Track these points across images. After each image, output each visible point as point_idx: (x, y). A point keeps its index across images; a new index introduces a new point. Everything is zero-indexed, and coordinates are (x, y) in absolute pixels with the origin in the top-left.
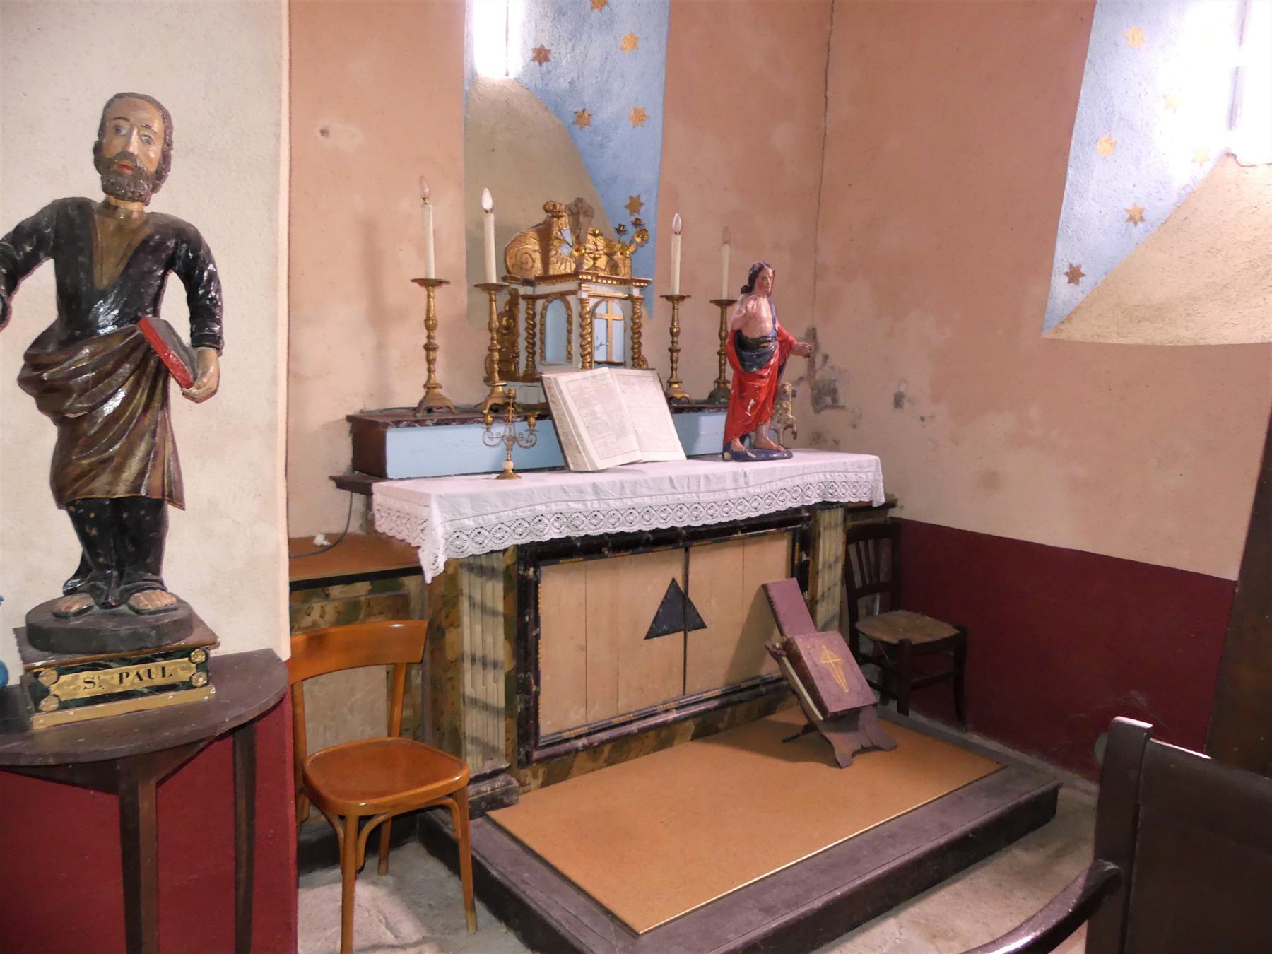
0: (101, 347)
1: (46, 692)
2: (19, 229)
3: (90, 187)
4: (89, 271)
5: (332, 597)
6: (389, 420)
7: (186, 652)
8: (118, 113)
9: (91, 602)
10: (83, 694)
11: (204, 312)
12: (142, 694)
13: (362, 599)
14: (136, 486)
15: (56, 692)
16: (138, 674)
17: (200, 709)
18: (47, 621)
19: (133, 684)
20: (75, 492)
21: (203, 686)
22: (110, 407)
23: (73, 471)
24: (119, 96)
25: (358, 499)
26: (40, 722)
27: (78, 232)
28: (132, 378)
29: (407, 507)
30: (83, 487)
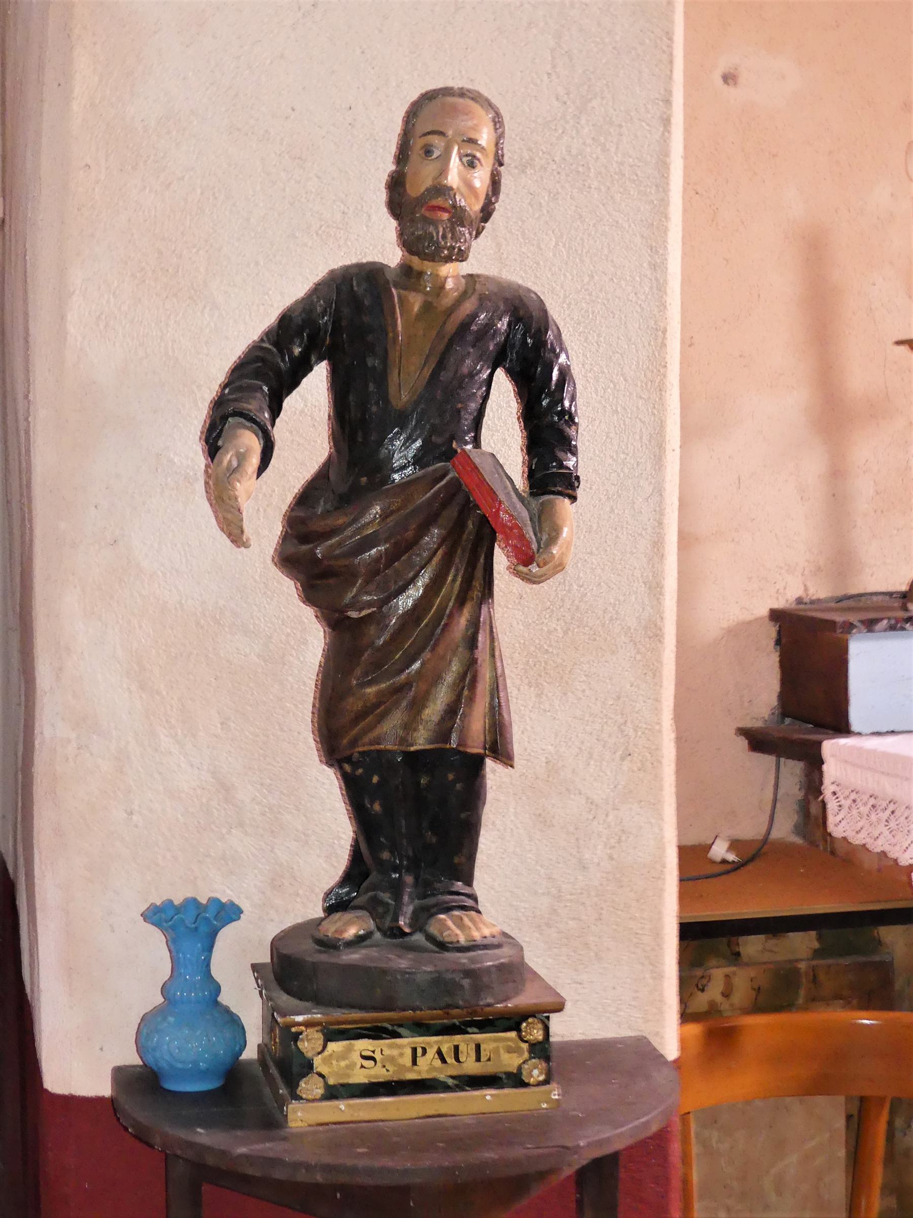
0: (397, 502)
1: (308, 1067)
2: (285, 320)
3: (379, 243)
4: (382, 378)
5: (745, 959)
6: (853, 618)
7: (512, 1022)
8: (428, 123)
9: (371, 925)
10: (360, 1077)
11: (548, 433)
12: (446, 1088)
13: (802, 966)
14: (443, 732)
15: (324, 1070)
16: (439, 1053)
17: (538, 1125)
18: (305, 949)
19: (432, 1068)
20: (354, 742)
21: (539, 1084)
22: (406, 602)
23: (353, 704)
24: (429, 97)
25: (793, 770)
26: (302, 1116)
27: (366, 319)
28: (440, 552)
29: (888, 787)
30: (365, 731)
